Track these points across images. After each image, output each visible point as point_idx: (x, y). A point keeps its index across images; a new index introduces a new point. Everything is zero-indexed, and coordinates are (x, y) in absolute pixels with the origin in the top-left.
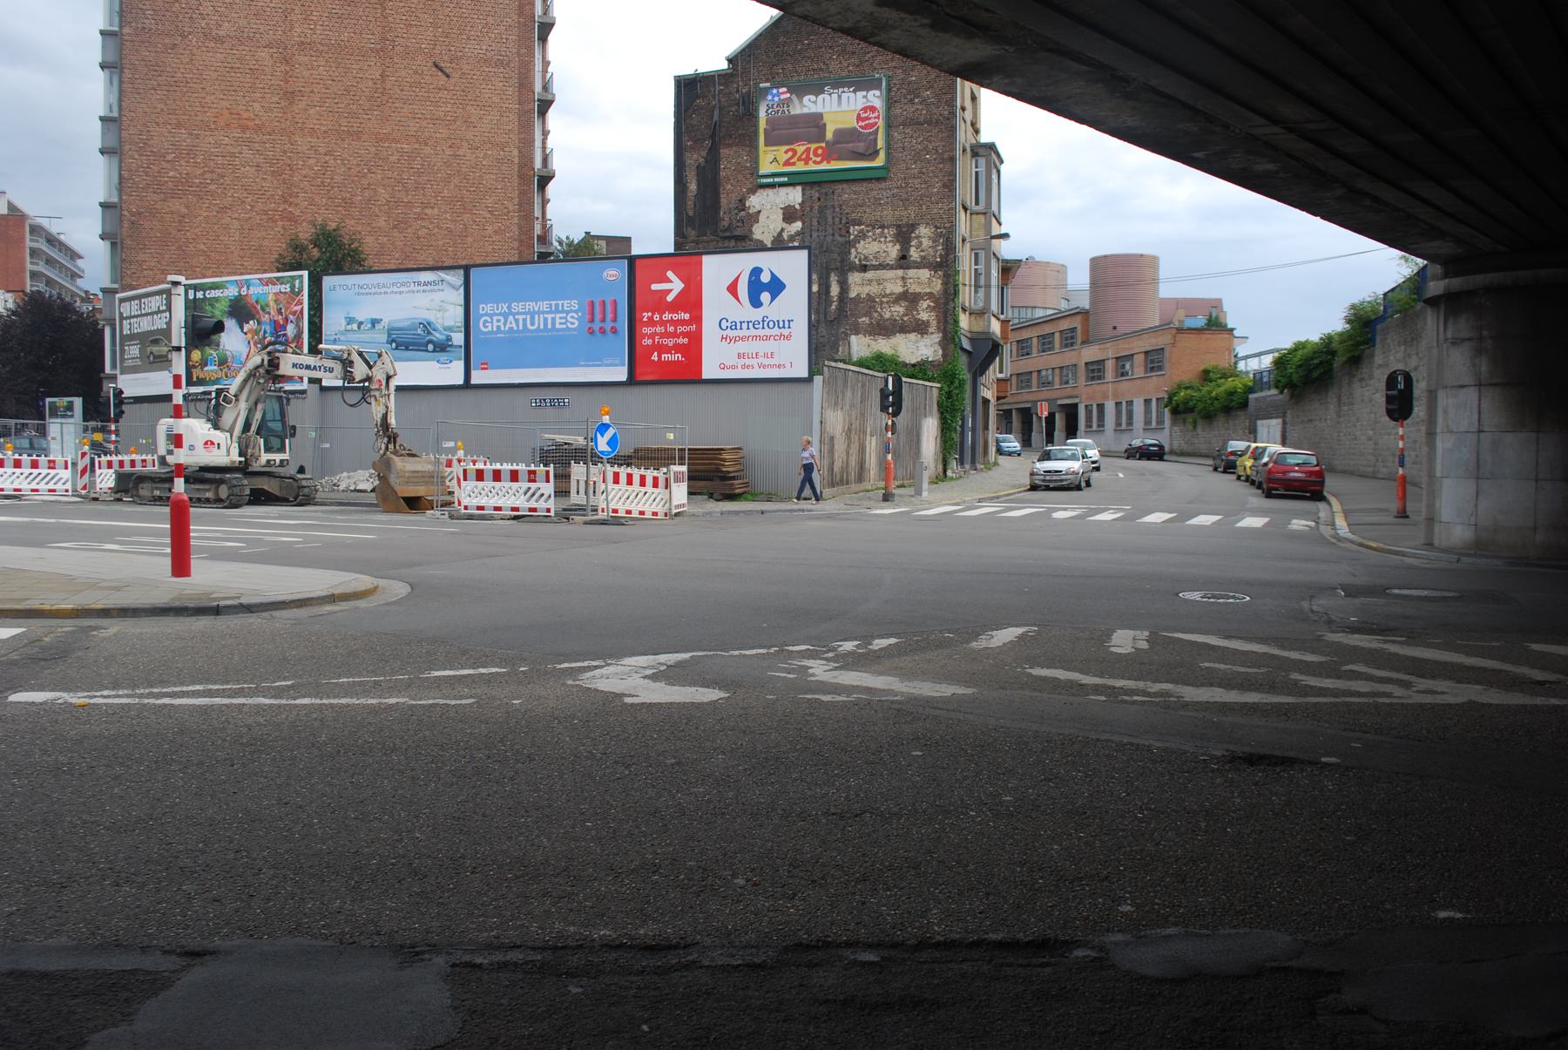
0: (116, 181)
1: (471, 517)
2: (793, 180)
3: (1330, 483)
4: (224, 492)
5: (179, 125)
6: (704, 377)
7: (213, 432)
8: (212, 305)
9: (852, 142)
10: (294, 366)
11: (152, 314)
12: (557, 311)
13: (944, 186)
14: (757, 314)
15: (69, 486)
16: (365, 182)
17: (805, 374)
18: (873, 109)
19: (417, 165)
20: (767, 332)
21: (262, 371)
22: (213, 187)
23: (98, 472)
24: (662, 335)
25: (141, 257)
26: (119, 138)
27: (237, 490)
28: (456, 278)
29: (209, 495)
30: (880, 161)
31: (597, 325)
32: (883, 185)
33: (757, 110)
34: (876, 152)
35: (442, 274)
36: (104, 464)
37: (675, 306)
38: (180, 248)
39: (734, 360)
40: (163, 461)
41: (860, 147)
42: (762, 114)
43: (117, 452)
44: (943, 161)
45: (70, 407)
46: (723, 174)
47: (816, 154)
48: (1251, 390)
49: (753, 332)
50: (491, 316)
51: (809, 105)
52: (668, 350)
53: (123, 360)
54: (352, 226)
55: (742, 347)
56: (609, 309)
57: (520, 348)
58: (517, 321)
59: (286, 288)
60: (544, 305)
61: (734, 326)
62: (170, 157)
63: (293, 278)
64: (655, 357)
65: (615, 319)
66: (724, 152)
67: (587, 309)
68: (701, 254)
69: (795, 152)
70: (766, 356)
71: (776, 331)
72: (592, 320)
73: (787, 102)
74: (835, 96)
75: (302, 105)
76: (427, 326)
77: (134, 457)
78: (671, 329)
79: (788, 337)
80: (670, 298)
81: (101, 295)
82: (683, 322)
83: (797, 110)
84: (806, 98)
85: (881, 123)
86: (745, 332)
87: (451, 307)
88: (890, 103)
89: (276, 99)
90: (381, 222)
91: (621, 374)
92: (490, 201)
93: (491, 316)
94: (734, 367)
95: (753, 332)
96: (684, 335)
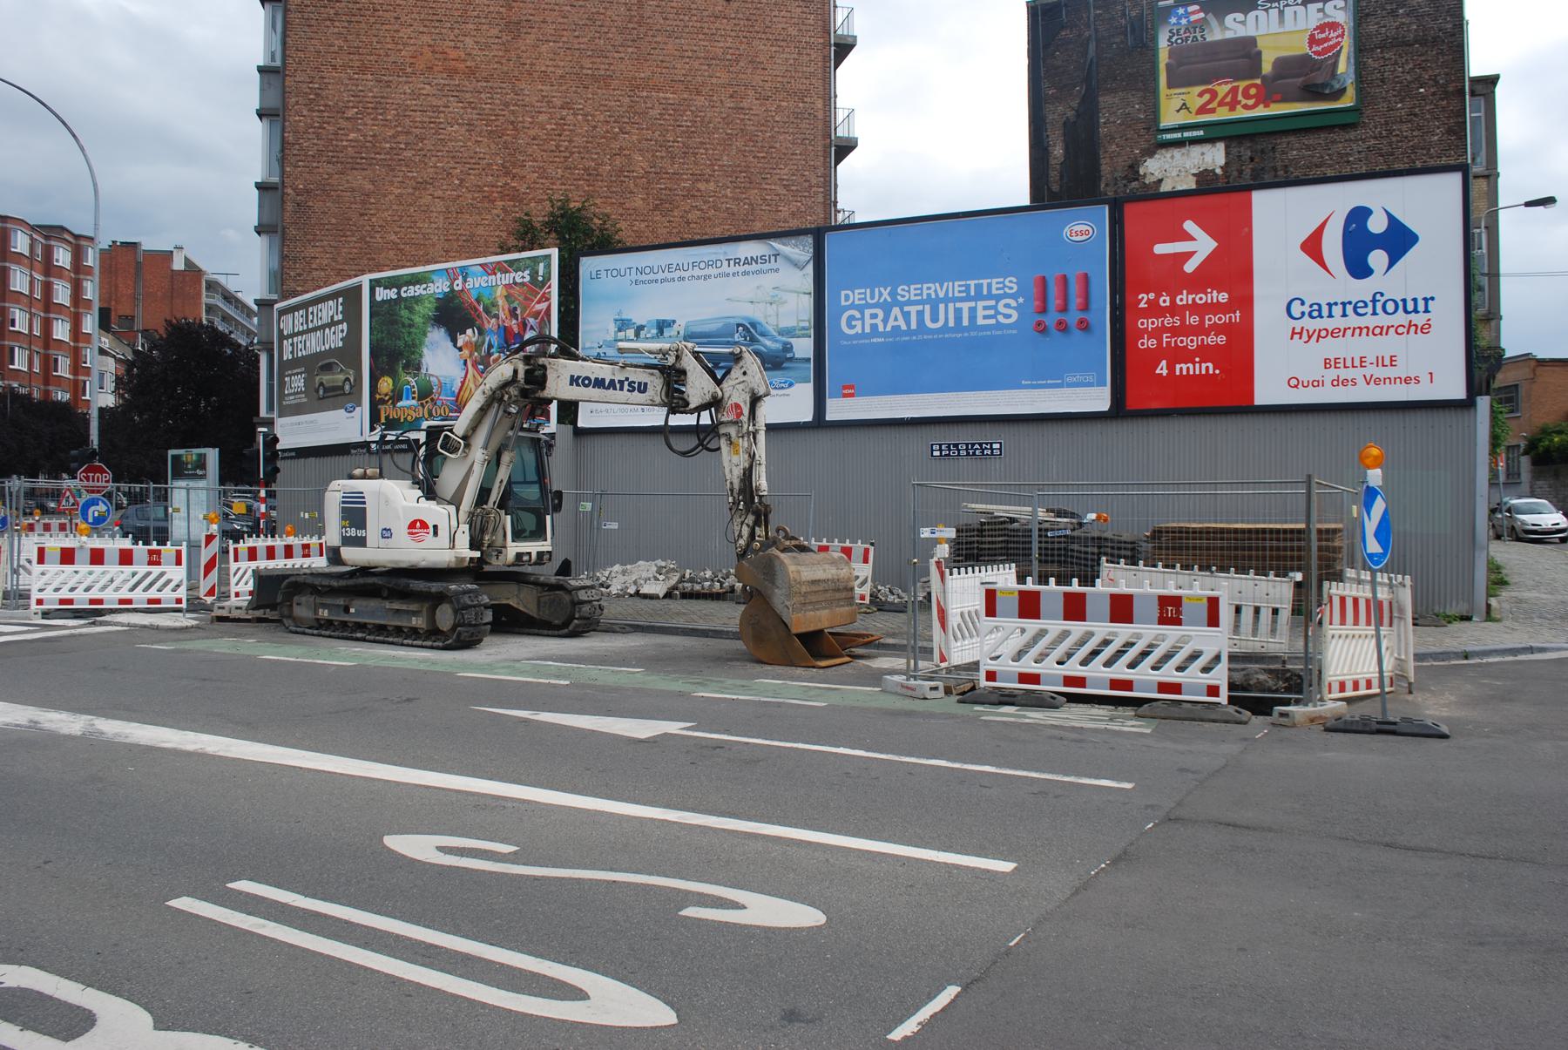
0: (278, 147)
1: (1006, 698)
2: (1212, 134)
4: (445, 617)
5: (363, 69)
6: (1260, 399)
7: (424, 503)
8: (410, 309)
9: (1305, 76)
10: (574, 381)
11: (323, 327)
12: (979, 296)
13: (1450, 131)
15: (182, 593)
16: (616, 145)
17: (1458, 391)
18: (1333, 26)
19: (686, 120)
20: (1383, 320)
21: (513, 391)
22: (408, 154)
23: (233, 566)
24: (1174, 332)
25: (310, 251)
26: (284, 92)
27: (469, 616)
28: (800, 250)
29: (418, 622)
31: (1051, 318)
32: (1352, 135)
33: (1154, 39)
34: (1343, 91)
35: (776, 245)
36: (243, 552)
37: (1199, 281)
38: (362, 239)
39: (1318, 371)
40: (335, 556)
42: (1163, 43)
43: (272, 531)
44: (1446, 95)
45: (201, 463)
46: (1103, 131)
49: (1353, 321)
50: (861, 309)
51: (1235, 26)
53: (282, 396)
54: (601, 208)
55: (1331, 348)
56: (1074, 289)
57: (912, 359)
58: (906, 316)
59: (524, 277)
60: (956, 288)
62: (350, 113)
63: (535, 260)
64: (1162, 369)
65: (1085, 307)
66: (1105, 100)
67: (1033, 290)
68: (1250, 188)
69: (1214, 94)
70: (1380, 362)
71: (1401, 318)
72: (1043, 310)
73: (1202, 25)
74: (1274, 13)
75: (530, 39)
76: (750, 331)
77: (291, 540)
78: (1193, 320)
79: (1425, 329)
80: (1190, 267)
81: (255, 308)
82: (1215, 308)
83: (1215, 34)
84: (1229, 19)
85: (1347, 44)
86: (1338, 322)
87: (792, 299)
89: (495, 32)
90: (638, 202)
91: (1100, 399)
92: (785, 172)
93: (861, 309)
94: (1317, 384)
96: (1218, 329)
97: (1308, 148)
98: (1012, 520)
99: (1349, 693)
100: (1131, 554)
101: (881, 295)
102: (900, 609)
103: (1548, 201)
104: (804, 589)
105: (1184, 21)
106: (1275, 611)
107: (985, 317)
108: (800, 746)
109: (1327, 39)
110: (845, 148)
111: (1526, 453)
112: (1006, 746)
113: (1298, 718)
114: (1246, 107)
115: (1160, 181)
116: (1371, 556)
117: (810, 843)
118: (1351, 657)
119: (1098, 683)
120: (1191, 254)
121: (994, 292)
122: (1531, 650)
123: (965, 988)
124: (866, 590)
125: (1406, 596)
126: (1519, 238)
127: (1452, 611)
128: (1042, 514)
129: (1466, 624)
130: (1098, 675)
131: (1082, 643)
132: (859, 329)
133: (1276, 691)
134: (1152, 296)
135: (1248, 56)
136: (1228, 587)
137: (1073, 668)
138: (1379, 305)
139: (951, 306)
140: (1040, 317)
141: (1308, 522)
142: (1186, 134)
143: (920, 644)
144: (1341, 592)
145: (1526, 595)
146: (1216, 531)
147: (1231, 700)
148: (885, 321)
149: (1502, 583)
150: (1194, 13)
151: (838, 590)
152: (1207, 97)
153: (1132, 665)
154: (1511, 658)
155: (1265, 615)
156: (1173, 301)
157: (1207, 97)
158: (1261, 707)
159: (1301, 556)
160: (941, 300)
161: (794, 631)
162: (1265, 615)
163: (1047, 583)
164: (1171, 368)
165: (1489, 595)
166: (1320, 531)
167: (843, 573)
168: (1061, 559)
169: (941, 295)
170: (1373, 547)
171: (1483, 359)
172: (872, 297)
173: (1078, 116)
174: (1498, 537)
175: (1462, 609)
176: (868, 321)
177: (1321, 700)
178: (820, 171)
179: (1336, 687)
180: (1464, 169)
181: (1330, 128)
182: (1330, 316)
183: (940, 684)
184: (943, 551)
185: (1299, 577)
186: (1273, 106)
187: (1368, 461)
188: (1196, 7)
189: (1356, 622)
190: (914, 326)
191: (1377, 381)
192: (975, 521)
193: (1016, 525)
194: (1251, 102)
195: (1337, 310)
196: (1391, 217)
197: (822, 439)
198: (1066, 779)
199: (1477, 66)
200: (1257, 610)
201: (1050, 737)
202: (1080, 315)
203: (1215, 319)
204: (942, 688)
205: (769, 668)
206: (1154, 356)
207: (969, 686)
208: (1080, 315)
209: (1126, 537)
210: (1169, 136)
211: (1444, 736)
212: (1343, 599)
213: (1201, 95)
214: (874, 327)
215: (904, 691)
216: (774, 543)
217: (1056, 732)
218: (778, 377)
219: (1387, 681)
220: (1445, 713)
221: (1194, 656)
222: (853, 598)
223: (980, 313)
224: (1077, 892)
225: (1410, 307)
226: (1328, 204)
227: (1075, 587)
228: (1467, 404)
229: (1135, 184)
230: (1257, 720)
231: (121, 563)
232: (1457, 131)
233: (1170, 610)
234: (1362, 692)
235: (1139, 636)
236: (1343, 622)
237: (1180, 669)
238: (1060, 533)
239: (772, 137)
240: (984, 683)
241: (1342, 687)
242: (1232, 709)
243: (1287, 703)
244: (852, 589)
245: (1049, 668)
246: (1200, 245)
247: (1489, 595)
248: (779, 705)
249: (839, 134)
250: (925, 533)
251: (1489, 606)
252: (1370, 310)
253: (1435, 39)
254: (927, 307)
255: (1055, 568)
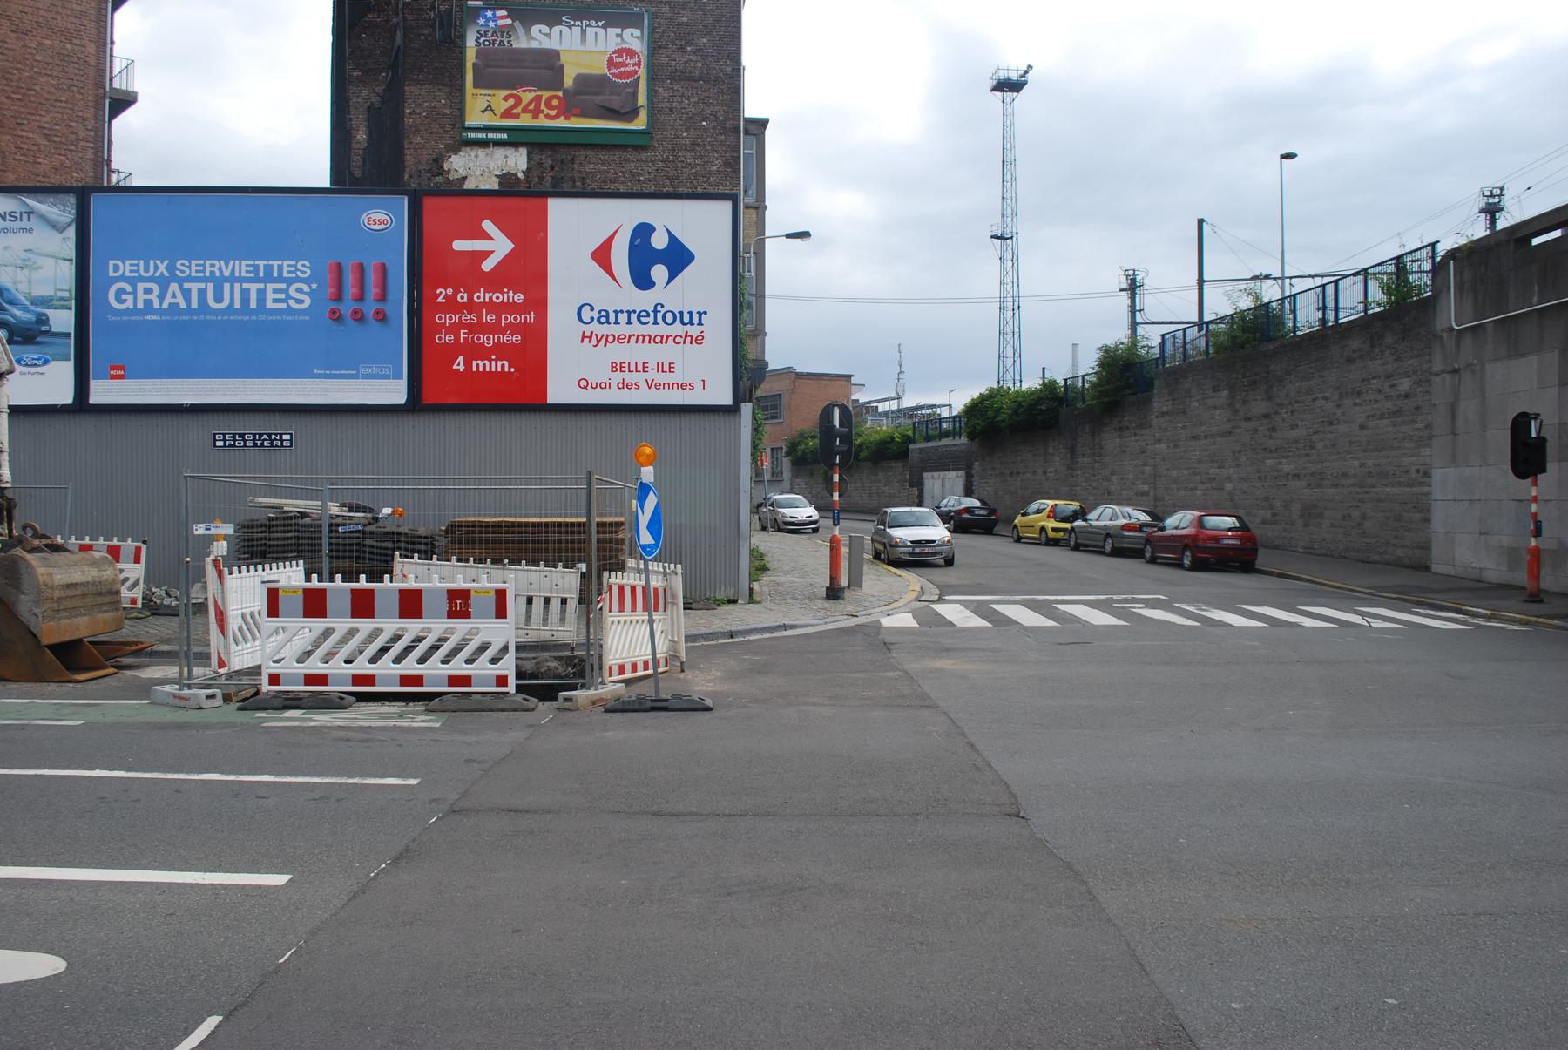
1: (291, 702)
3: (1262, 560)
6: (553, 397)
9: (592, 93)
12: (268, 278)
13: (726, 164)
14: (644, 300)
17: (726, 399)
18: (631, 53)
20: (662, 329)
24: (472, 329)
28: (61, 211)
30: (640, 123)
31: (347, 307)
32: (643, 156)
33: (463, 37)
34: (632, 114)
37: (497, 280)
39: (604, 374)
41: (615, 102)
42: (471, 42)
44: (724, 131)
46: (408, 121)
47: (549, 106)
48: (910, 440)
49: (637, 328)
50: (133, 282)
51: (540, 37)
52: (483, 353)
55: (618, 352)
56: (371, 278)
57: (190, 340)
58: (186, 294)
60: (243, 267)
61: (603, 318)
64: (459, 365)
65: (382, 298)
66: (411, 90)
68: (546, 195)
69: (518, 100)
70: (660, 368)
71: (678, 329)
72: (338, 297)
73: (508, 31)
74: (576, 30)
78: (490, 318)
79: (699, 340)
80: (488, 265)
83: (521, 42)
84: (535, 29)
85: (642, 72)
87: (48, 264)
88: (654, 48)
91: (396, 392)
93: (133, 282)
94: (604, 386)
95: (637, 328)
96: (514, 329)
97: (604, 164)
98: (303, 515)
99: (628, 675)
100: (425, 548)
101: (157, 268)
102: (172, 613)
103: (804, 235)
104: (57, 594)
105: (492, 24)
106: (564, 601)
107: (275, 301)
108: (47, 772)
109: (624, 64)
110: (123, 102)
111: (787, 455)
112: (288, 753)
113: (580, 702)
114: (548, 117)
115: (464, 178)
116: (644, 547)
117: (50, 882)
118: (629, 641)
119: (387, 680)
120: (489, 253)
121: (285, 275)
122: (784, 627)
123: (227, 1017)
124: (138, 593)
125: (678, 584)
126: (782, 266)
127: (721, 596)
128: (334, 508)
129: (732, 606)
130: (387, 671)
131: (372, 637)
132: (130, 304)
133: (567, 677)
134: (450, 291)
135: (551, 68)
136: (517, 579)
137: (362, 667)
138: (659, 316)
139: (237, 286)
140: (333, 305)
141: (589, 516)
142: (490, 136)
143: (196, 649)
144: (619, 581)
145: (782, 579)
146: (508, 525)
147: (519, 689)
148: (162, 297)
149: (764, 569)
150: (502, 18)
151: (100, 594)
152: (511, 102)
153: (422, 660)
154: (768, 635)
155: (555, 605)
156: (470, 298)
157: (511, 102)
158: (548, 694)
159: (589, 548)
160: (227, 280)
161: (45, 641)
162: (555, 605)
163: (332, 580)
164: (468, 364)
165: (752, 580)
166: (598, 524)
167: (108, 574)
168: (355, 554)
169: (227, 273)
170: (646, 538)
171: (748, 371)
172: (147, 270)
173: (383, 103)
174: (764, 528)
175: (730, 593)
176: (141, 297)
177: (603, 683)
178: (90, 124)
179: (616, 670)
180: (735, 200)
181: (624, 147)
182: (617, 322)
183: (217, 691)
184: (221, 548)
185: (583, 567)
186: (573, 119)
187: (642, 459)
188: (504, 13)
189: (634, 609)
190: (194, 305)
191: (658, 386)
192: (263, 516)
193: (307, 520)
194: (553, 113)
195: (623, 318)
196: (670, 234)
197: (85, 426)
198: (350, 781)
199: (752, 108)
200: (547, 601)
201: (335, 739)
202: (355, 305)
203: (511, 319)
204: (219, 696)
205: (14, 685)
206: (452, 351)
207: (252, 691)
208: (355, 305)
209: (422, 531)
210: (473, 135)
211: (709, 709)
212: (621, 588)
213: (506, 99)
214: (148, 303)
215: (177, 702)
216: (20, 542)
217: (342, 734)
218: (29, 353)
219: (662, 662)
220: (711, 687)
221: (483, 648)
222: (119, 602)
223: (270, 296)
224: (354, 897)
225: (686, 320)
226: (615, 217)
227: (363, 583)
228: (732, 410)
229: (438, 179)
230: (544, 706)
231: (419, 592)
232: (733, 164)
233: (459, 604)
234: (640, 673)
235: (429, 630)
236: (622, 609)
237: (469, 661)
238: (352, 528)
239: (31, 78)
240: (266, 687)
241: (622, 670)
242: (520, 697)
243: (574, 687)
244: (118, 592)
245: (336, 668)
246: (498, 246)
247: (752, 580)
248: (23, 727)
249: (116, 85)
250: (199, 529)
251: (751, 590)
252: (651, 319)
253: (717, 79)
254: (211, 286)
255: (341, 564)
